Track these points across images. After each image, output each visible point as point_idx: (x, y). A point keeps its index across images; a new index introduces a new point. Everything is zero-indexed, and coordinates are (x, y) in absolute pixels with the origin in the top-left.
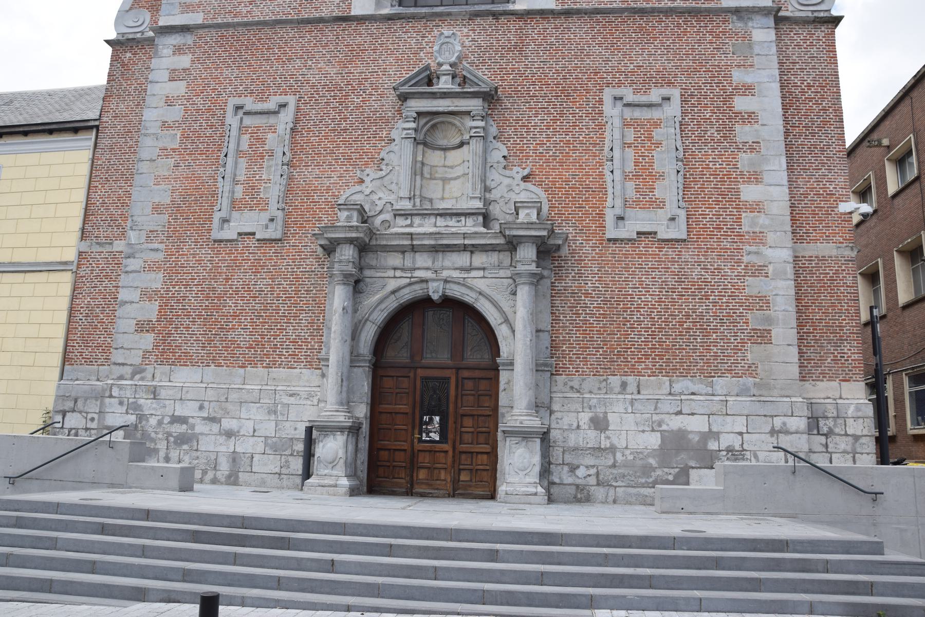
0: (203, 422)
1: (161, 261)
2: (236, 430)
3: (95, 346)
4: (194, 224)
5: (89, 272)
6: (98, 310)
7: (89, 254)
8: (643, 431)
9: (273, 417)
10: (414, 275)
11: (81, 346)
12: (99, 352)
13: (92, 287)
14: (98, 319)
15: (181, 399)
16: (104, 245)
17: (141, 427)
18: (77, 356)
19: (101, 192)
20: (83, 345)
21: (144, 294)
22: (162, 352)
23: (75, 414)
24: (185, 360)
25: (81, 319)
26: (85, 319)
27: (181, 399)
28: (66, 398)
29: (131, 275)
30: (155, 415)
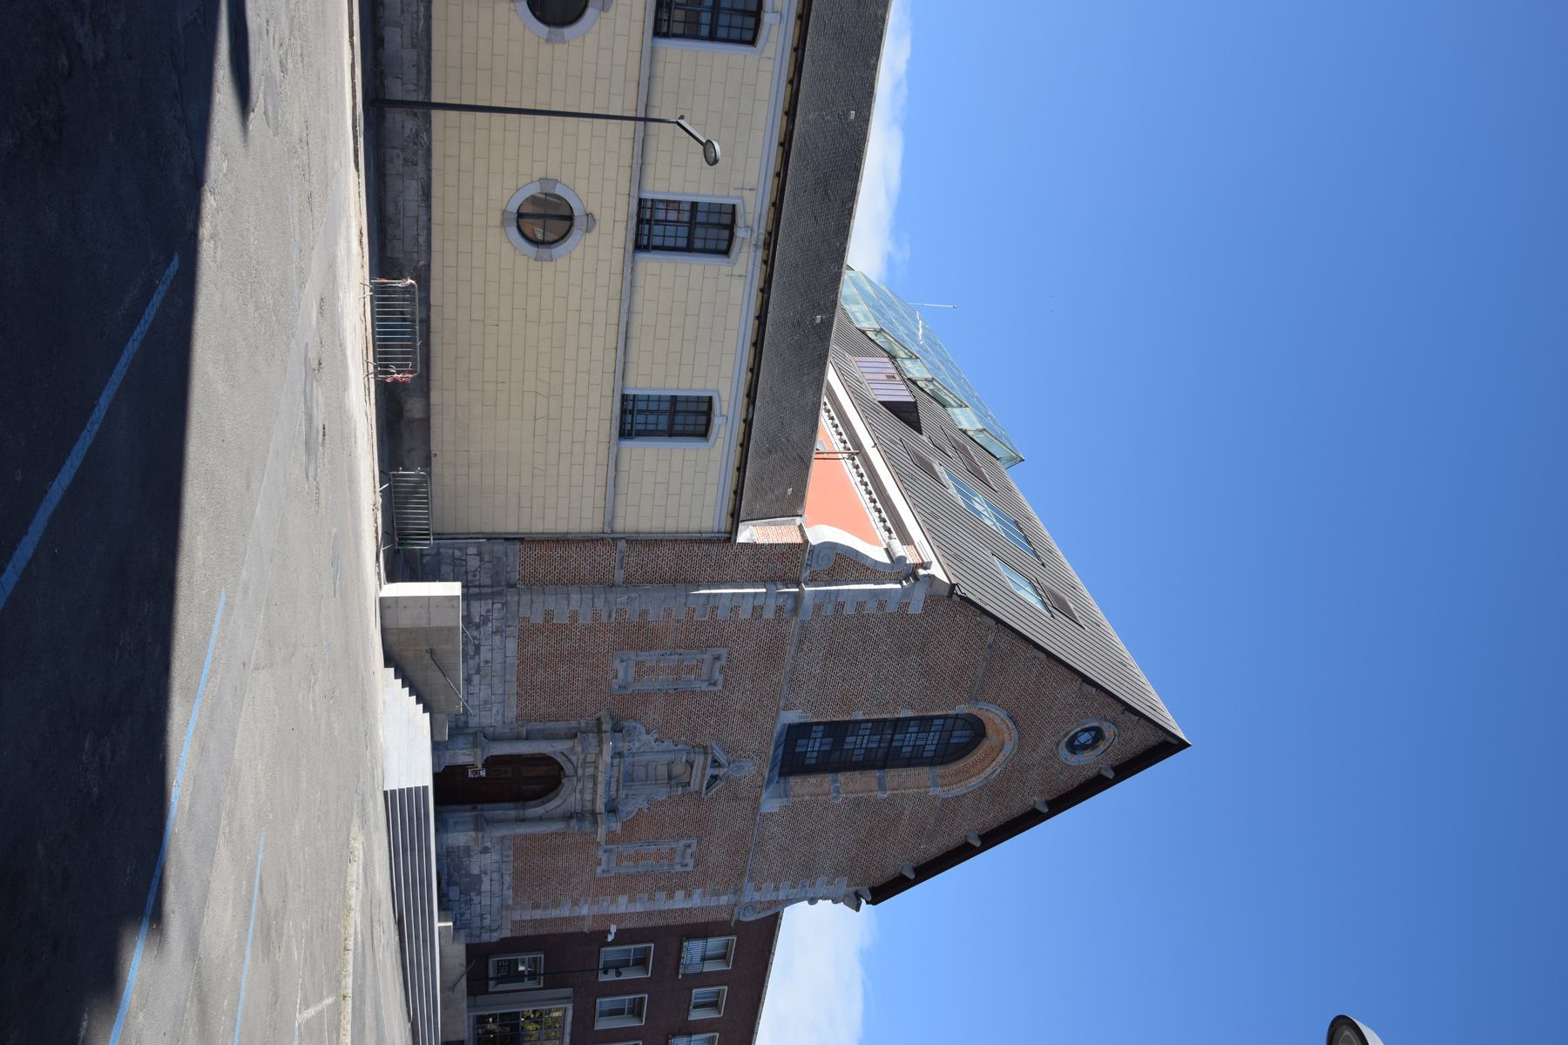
24: (522, 643)
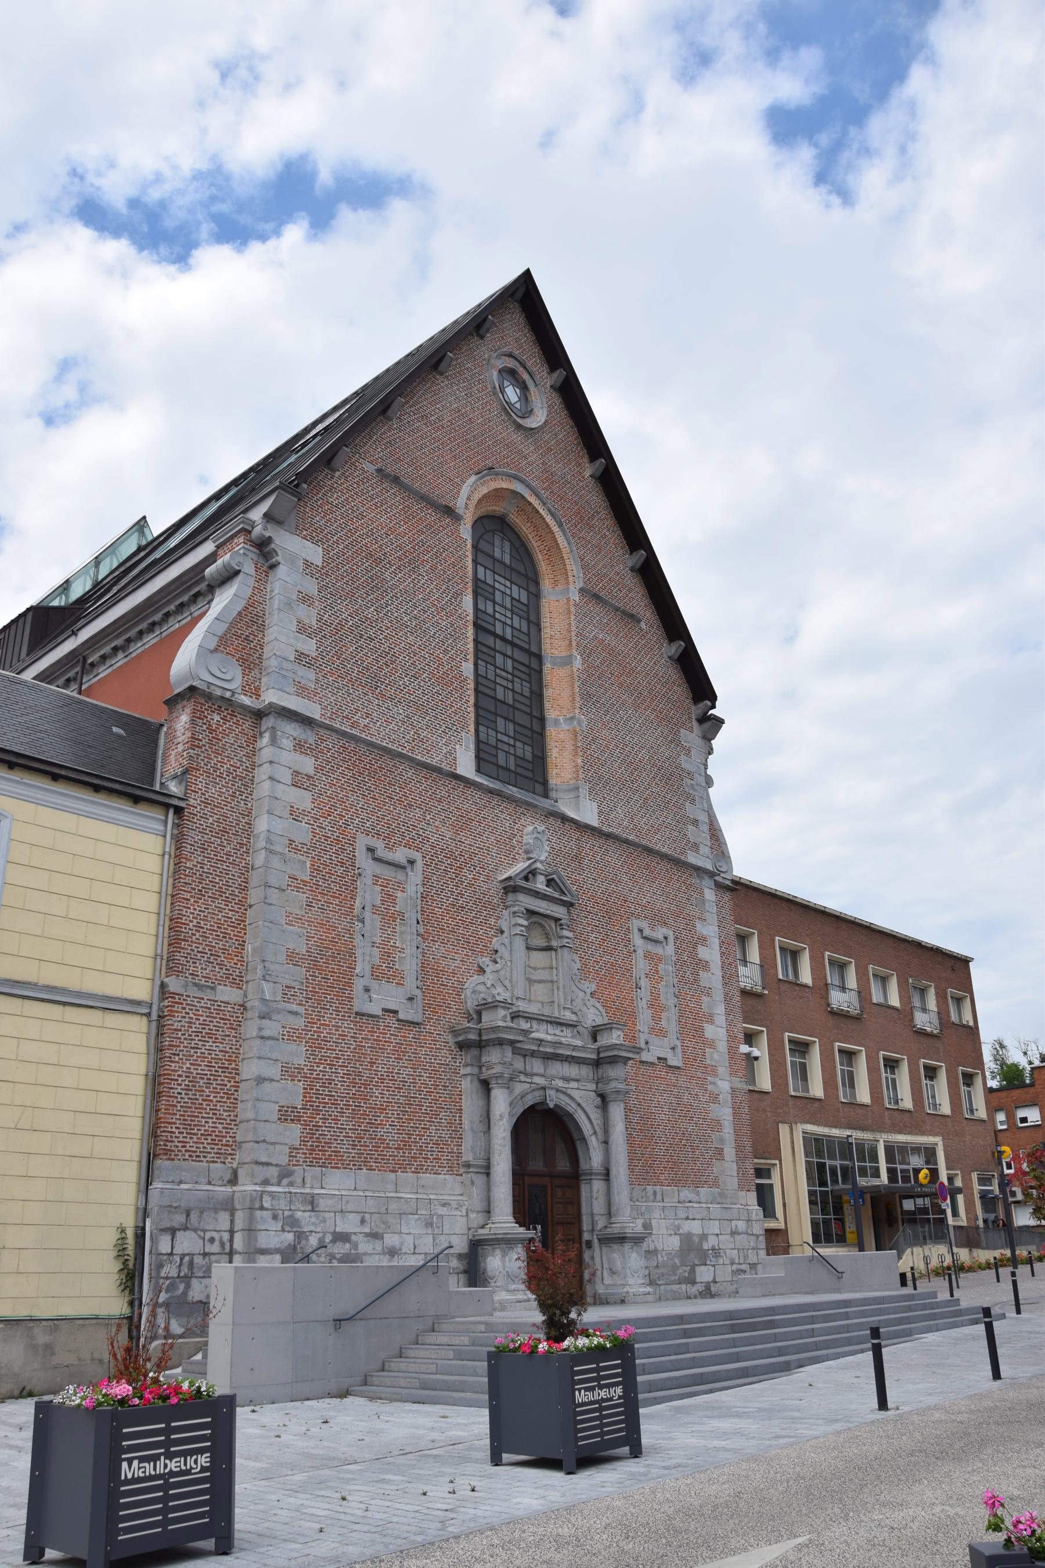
0: (366, 1239)
1: (302, 1030)
2: (398, 1248)
3: (202, 1135)
4: (333, 987)
5: (186, 1025)
6: (202, 1082)
7: (184, 997)
8: (671, 1235)
9: (430, 1231)
10: (534, 1081)
11: (183, 1133)
12: (208, 1144)
13: (191, 1048)
14: (203, 1095)
15: (342, 1211)
16: (204, 988)
17: (301, 1248)
18: (177, 1147)
19: (195, 909)
20: (185, 1131)
21: (286, 1071)
22: (311, 1150)
23: (188, 1233)
25: (180, 1094)
26: (186, 1094)
27: (342, 1211)
28: (173, 1210)
29: (268, 1042)
30: (316, 1232)
